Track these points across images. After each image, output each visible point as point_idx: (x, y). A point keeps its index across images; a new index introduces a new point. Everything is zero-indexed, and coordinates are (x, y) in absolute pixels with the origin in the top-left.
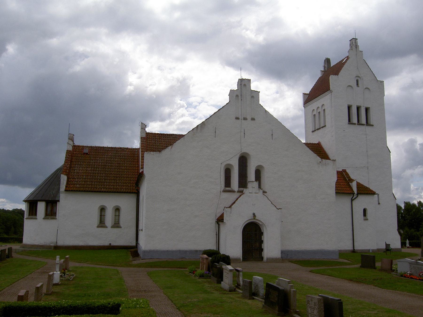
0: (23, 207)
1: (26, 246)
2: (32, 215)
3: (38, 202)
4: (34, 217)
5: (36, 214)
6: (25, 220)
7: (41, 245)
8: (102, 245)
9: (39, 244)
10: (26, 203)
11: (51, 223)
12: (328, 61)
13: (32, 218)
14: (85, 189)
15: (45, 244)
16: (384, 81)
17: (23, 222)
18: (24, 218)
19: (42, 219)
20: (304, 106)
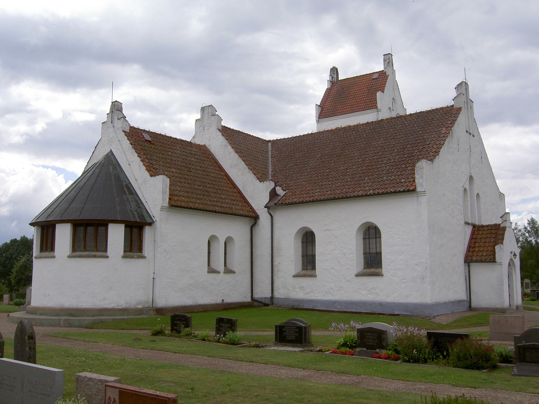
0: (32, 233)
1: (35, 311)
2: (46, 250)
3: (109, 224)
4: (51, 254)
5: (52, 249)
6: (34, 259)
7: (119, 307)
8: (214, 302)
9: (116, 307)
10: (36, 227)
11: (135, 264)
12: (334, 71)
13: (46, 257)
14: (201, 206)
15: (128, 305)
16: (216, 111)
17: (32, 262)
18: (32, 256)
19: (121, 258)
20: (318, 122)
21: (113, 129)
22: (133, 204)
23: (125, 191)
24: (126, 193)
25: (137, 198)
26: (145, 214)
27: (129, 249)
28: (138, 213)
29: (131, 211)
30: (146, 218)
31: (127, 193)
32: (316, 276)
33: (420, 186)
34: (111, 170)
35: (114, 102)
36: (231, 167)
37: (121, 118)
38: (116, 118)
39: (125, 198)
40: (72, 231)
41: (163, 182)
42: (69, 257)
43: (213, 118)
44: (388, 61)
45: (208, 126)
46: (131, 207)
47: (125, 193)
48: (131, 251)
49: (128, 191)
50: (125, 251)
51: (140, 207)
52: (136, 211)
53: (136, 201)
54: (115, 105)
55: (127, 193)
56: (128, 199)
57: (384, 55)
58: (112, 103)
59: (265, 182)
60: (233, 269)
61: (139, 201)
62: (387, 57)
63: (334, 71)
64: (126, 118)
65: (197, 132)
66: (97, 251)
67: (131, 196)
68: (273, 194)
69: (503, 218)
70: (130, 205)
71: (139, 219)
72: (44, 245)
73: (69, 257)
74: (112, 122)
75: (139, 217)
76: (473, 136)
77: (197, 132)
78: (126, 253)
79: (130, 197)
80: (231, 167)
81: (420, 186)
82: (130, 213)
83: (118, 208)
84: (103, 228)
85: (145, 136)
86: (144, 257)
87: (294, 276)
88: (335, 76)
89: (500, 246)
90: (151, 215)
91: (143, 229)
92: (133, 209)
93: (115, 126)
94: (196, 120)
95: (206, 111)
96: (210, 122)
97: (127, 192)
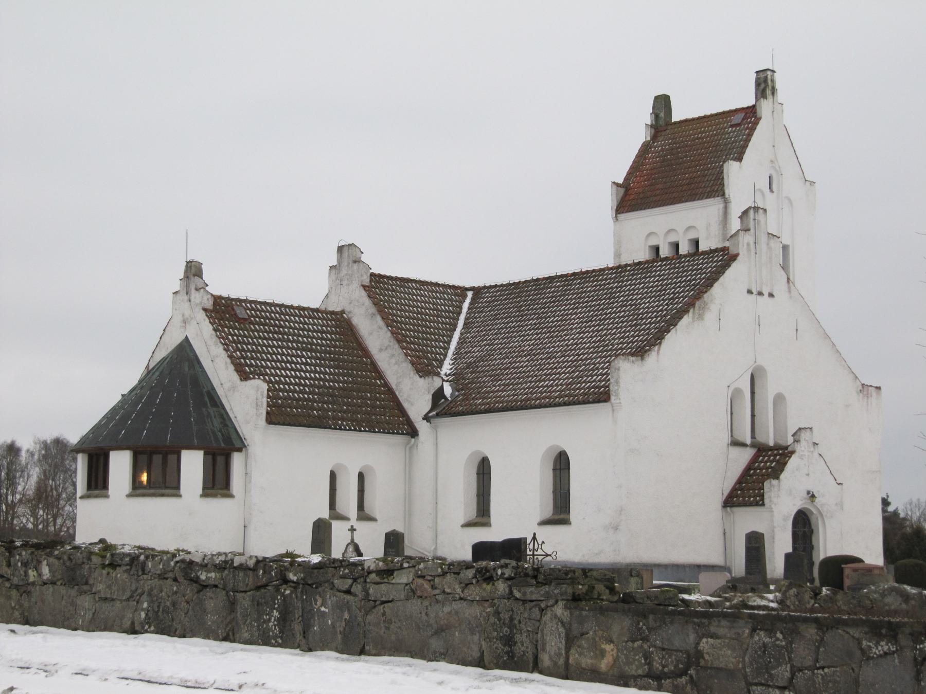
2: (96, 488)
5: (105, 486)
6: (78, 499)
11: (218, 505)
12: (663, 103)
21: (187, 304)
22: (217, 422)
23: (206, 402)
24: (207, 404)
25: (222, 411)
26: (234, 436)
27: (211, 485)
28: (223, 435)
29: (213, 432)
30: (234, 442)
31: (209, 405)
32: (491, 526)
33: (614, 394)
34: (187, 369)
35: (190, 262)
36: (381, 350)
37: (200, 289)
38: (193, 287)
39: (205, 413)
40: (132, 460)
41: (258, 390)
42: (129, 496)
43: (355, 266)
44: (763, 86)
45: (348, 279)
46: (213, 426)
47: (205, 405)
48: (213, 487)
49: (210, 402)
50: (204, 488)
51: (226, 425)
52: (220, 431)
53: (222, 416)
54: (191, 267)
55: (209, 405)
56: (209, 413)
57: (757, 72)
58: (187, 262)
59: (426, 378)
60: (373, 515)
61: (225, 416)
62: (762, 75)
63: (663, 103)
64: (207, 288)
65: (331, 288)
66: (166, 488)
67: (214, 409)
68: (438, 395)
69: (795, 437)
70: (212, 423)
71: (225, 444)
72: (93, 479)
73: (129, 496)
74: (187, 294)
75: (224, 440)
76: (771, 295)
77: (331, 288)
78: (206, 491)
79: (212, 411)
80: (381, 350)
81: (614, 394)
82: (211, 434)
83: (195, 428)
84: (175, 456)
85: (238, 312)
86: (231, 496)
87: (463, 526)
88: (662, 115)
89: (770, 482)
90: (242, 436)
91: (230, 457)
92: (215, 429)
93: (192, 300)
94: (330, 267)
95: (345, 254)
96: (350, 272)
97: (208, 403)
